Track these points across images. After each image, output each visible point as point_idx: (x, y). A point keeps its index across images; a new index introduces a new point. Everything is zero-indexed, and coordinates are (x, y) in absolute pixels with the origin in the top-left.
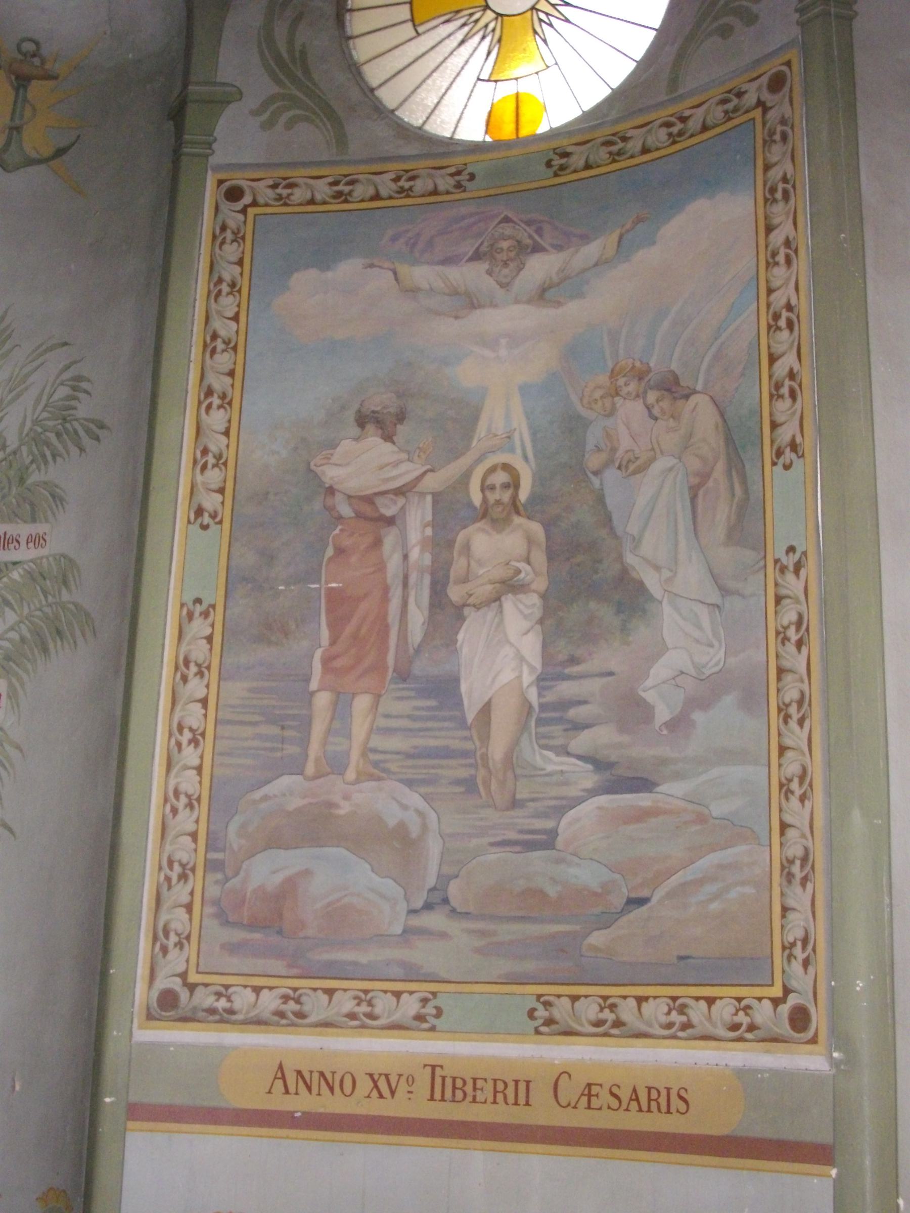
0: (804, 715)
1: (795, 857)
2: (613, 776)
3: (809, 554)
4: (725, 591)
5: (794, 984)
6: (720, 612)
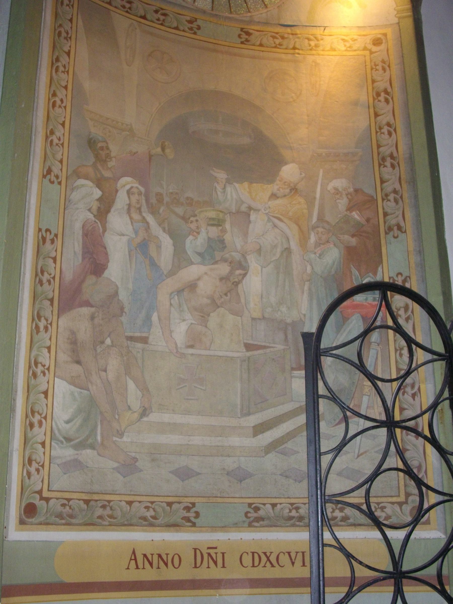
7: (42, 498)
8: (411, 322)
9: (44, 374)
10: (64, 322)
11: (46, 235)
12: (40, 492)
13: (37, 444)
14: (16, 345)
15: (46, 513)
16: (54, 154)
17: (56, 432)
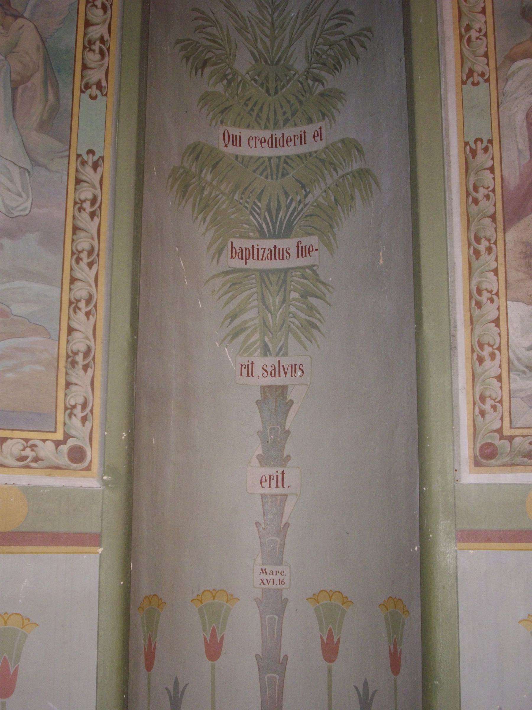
0: (93, 261)
1: (79, 351)
2: (230, 267)
3: (105, 159)
4: (34, 162)
5: (73, 432)
6: (29, 175)
7: (502, 437)
8: (96, 220)
9: (492, 301)
10: (511, 236)
11: (476, 146)
12: (500, 431)
13: (491, 379)
14: (449, 278)
15: (510, 452)
16: (473, 51)
17: (515, 362)
